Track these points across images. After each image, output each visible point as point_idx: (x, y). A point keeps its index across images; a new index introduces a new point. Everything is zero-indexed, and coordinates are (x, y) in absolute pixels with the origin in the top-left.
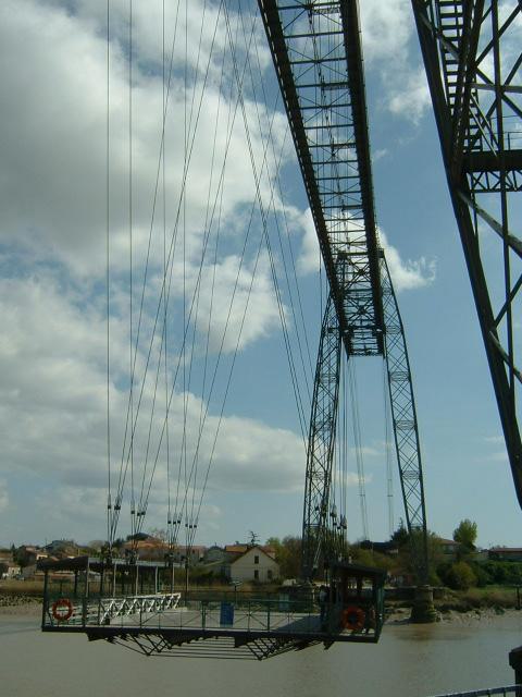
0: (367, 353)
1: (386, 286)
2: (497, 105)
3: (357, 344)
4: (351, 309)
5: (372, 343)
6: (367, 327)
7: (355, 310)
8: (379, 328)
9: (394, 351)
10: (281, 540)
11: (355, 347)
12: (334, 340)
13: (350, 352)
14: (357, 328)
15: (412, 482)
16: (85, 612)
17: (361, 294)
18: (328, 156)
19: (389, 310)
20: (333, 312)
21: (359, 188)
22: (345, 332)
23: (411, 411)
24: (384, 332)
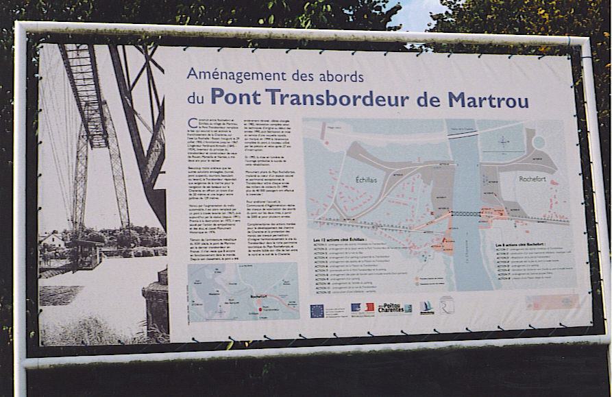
0: (99, 146)
1: (108, 117)
2: (147, 65)
3: (95, 142)
4: (91, 127)
5: (103, 143)
6: (100, 135)
7: (93, 127)
8: (105, 134)
9: (113, 145)
10: (150, 227)
11: (94, 144)
12: (84, 141)
13: (92, 146)
14: (95, 135)
15: (119, 181)
16: (543, 14)
17: (95, 120)
18: (75, 56)
19: (109, 127)
20: (84, 129)
21: (91, 70)
22: (90, 137)
23: (127, 216)
24: (108, 137)
